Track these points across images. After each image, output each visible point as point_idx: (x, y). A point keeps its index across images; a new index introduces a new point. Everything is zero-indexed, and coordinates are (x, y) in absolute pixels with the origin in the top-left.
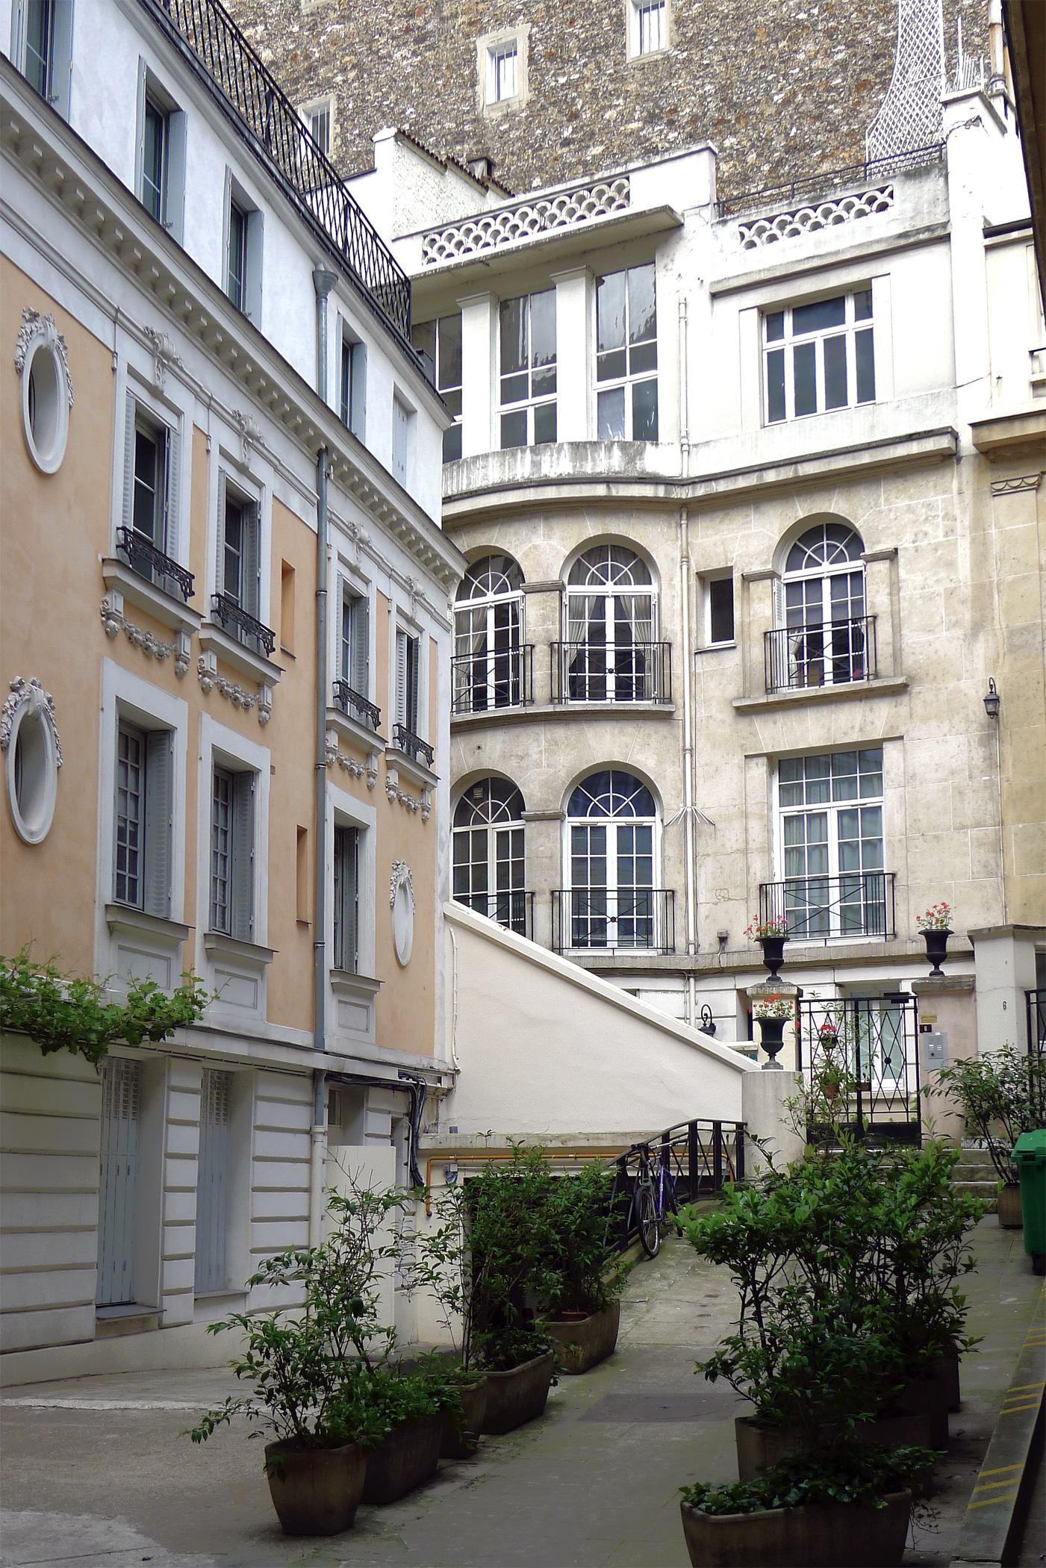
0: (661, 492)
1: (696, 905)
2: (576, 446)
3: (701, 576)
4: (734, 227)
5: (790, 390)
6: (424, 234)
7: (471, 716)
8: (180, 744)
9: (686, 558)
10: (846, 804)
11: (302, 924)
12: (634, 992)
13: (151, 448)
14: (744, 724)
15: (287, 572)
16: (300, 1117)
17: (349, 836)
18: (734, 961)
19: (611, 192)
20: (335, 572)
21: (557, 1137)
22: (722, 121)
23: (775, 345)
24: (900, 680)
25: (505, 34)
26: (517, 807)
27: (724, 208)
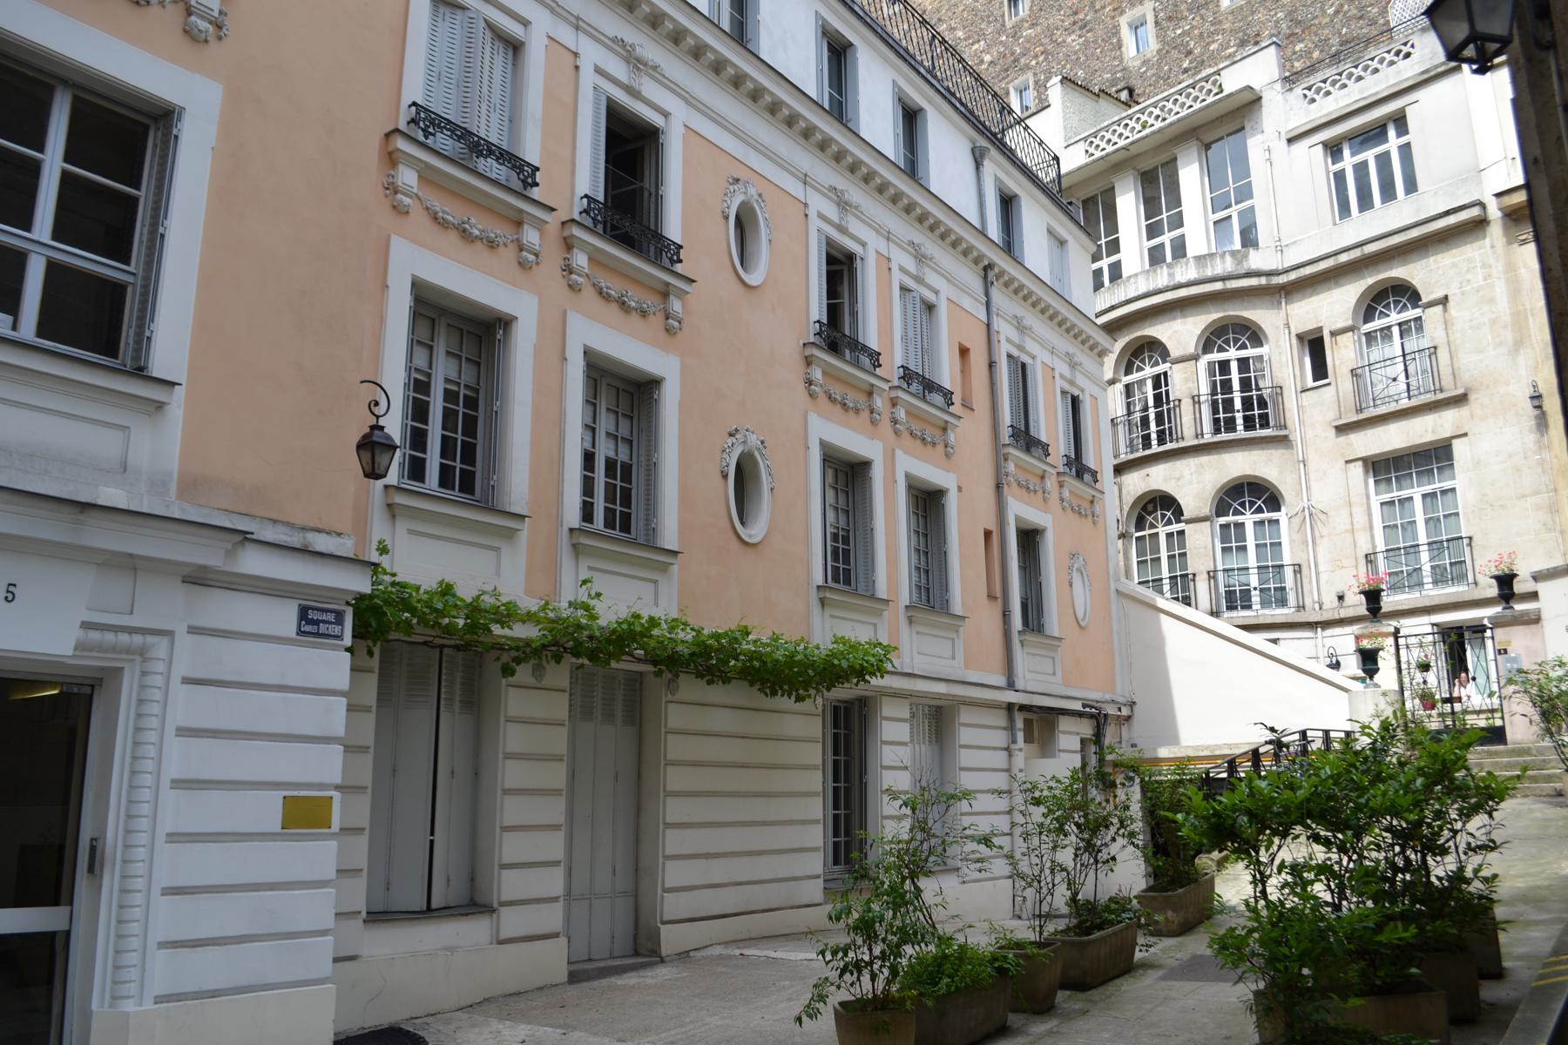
0: (1263, 281)
1: (1317, 574)
2: (1198, 258)
3: (1300, 337)
4: (1299, 91)
5: (1350, 196)
6: (1085, 139)
7: (1141, 453)
8: (877, 474)
9: (1287, 325)
10: (1428, 489)
11: (991, 597)
12: (1275, 641)
13: (840, 269)
14: (1343, 439)
15: (964, 352)
16: (1000, 738)
17: (1030, 538)
18: (1350, 613)
19: (1208, 86)
20: (1004, 349)
21: (1207, 748)
22: (1293, 34)
23: (1338, 166)
24: (1460, 391)
25: (1137, 11)
26: (1178, 513)
27: (1290, 80)
